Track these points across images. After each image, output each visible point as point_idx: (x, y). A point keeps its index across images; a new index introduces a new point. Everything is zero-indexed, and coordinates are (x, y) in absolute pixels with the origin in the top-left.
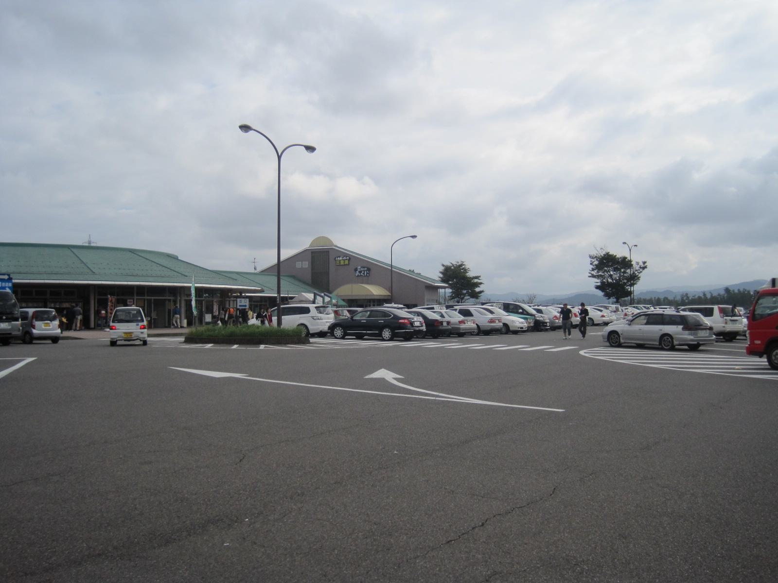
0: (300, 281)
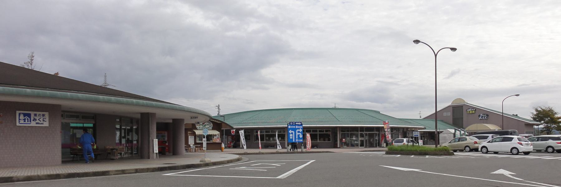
0: (446, 123)
